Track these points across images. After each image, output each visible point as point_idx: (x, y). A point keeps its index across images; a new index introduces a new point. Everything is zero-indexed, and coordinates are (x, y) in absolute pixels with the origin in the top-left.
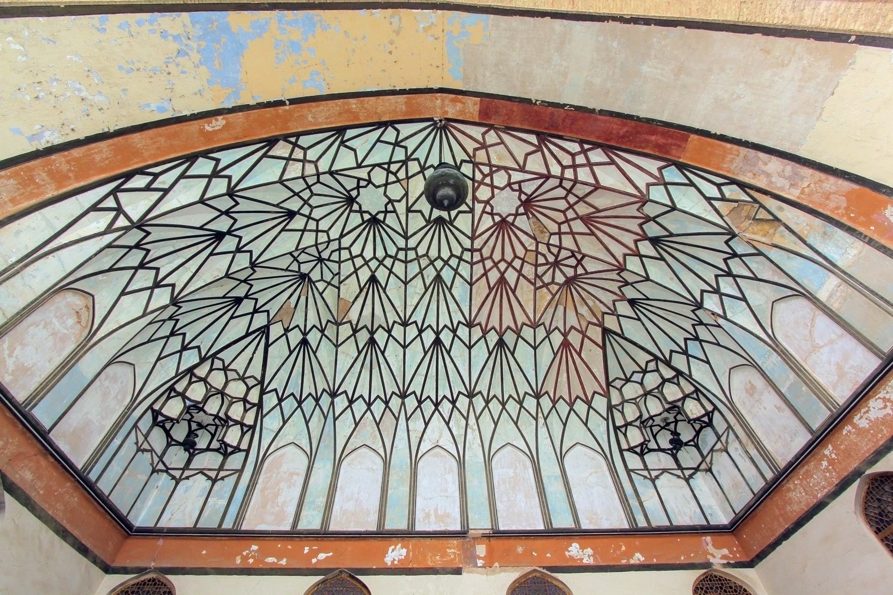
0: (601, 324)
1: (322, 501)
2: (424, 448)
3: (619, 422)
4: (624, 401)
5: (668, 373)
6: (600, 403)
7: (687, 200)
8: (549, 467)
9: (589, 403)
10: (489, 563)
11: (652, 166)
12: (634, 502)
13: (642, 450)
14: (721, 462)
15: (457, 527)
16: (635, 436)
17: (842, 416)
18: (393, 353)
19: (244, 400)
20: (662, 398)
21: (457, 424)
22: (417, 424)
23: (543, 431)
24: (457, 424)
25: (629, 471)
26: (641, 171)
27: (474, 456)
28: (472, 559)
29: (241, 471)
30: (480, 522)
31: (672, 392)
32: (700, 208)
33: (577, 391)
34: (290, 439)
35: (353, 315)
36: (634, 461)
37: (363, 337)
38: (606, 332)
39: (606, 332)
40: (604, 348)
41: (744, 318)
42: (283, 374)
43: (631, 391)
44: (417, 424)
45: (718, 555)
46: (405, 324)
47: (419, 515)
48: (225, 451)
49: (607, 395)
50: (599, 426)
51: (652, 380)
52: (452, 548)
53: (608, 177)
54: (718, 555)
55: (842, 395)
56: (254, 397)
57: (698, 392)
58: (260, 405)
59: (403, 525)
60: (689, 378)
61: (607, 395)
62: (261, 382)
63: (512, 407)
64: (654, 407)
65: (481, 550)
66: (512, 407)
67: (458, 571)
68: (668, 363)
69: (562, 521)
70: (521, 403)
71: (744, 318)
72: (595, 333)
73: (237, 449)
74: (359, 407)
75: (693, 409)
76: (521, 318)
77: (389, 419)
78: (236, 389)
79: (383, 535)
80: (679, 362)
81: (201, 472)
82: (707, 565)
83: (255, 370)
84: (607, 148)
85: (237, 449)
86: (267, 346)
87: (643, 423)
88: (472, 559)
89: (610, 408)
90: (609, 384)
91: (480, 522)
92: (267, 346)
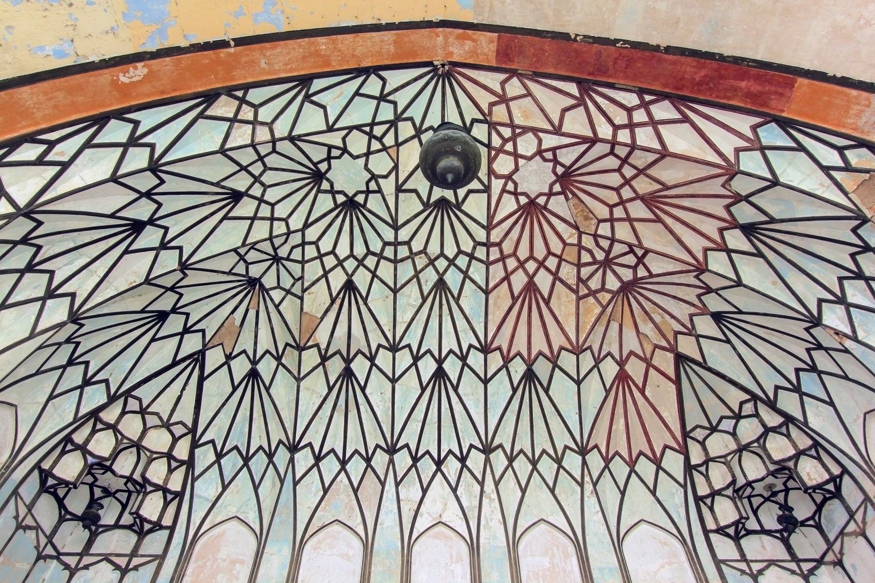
0: (672, 349)
5: (772, 420)
7: (795, 171)
11: (743, 123)
20: (764, 455)
21: (468, 490)
26: (726, 132)
31: (779, 447)
36: (725, 548)
38: (681, 359)
39: (681, 359)
43: (719, 444)
44: (411, 492)
51: (749, 430)
53: (680, 139)
57: (818, 447)
60: (804, 426)
61: (685, 451)
68: (772, 405)
72: (665, 361)
75: (811, 471)
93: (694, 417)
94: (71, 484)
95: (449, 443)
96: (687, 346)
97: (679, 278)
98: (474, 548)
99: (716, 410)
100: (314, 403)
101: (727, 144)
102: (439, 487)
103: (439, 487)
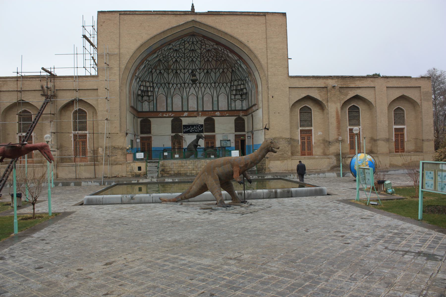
1: (171, 106)
2: (190, 94)
3: (232, 89)
4: (234, 85)
6: (229, 84)
8: (215, 99)
9: (227, 84)
10: (202, 115)
12: (230, 105)
13: (235, 95)
15: (196, 110)
16: (234, 92)
18: (182, 75)
19: (150, 86)
22: (188, 89)
23: (215, 91)
25: (231, 99)
27: (200, 96)
28: (198, 115)
29: (153, 100)
30: (200, 109)
33: (225, 81)
34: (161, 92)
35: (172, 67)
36: (233, 97)
37: (174, 71)
38: (233, 70)
39: (233, 70)
40: (232, 73)
42: (157, 79)
43: (236, 83)
44: (188, 89)
46: (184, 69)
47: (189, 107)
48: (149, 96)
49: (231, 83)
50: (228, 89)
51: (240, 82)
52: (195, 114)
54: (241, 114)
56: (151, 85)
58: (153, 86)
59: (186, 110)
61: (231, 83)
62: (152, 82)
65: (200, 113)
66: (209, 85)
67: (196, 117)
68: (153, 84)
70: (211, 84)
73: (151, 96)
74: (175, 85)
76: (212, 67)
77: (181, 88)
78: (148, 84)
79: (183, 112)
80: (155, 85)
81: (146, 100)
82: (239, 116)
83: (151, 80)
85: (151, 96)
86: (152, 74)
89: (231, 86)
90: (232, 81)
91: (200, 109)
92: (152, 74)
93: (233, 78)
95: (206, 81)
102: (192, 89)
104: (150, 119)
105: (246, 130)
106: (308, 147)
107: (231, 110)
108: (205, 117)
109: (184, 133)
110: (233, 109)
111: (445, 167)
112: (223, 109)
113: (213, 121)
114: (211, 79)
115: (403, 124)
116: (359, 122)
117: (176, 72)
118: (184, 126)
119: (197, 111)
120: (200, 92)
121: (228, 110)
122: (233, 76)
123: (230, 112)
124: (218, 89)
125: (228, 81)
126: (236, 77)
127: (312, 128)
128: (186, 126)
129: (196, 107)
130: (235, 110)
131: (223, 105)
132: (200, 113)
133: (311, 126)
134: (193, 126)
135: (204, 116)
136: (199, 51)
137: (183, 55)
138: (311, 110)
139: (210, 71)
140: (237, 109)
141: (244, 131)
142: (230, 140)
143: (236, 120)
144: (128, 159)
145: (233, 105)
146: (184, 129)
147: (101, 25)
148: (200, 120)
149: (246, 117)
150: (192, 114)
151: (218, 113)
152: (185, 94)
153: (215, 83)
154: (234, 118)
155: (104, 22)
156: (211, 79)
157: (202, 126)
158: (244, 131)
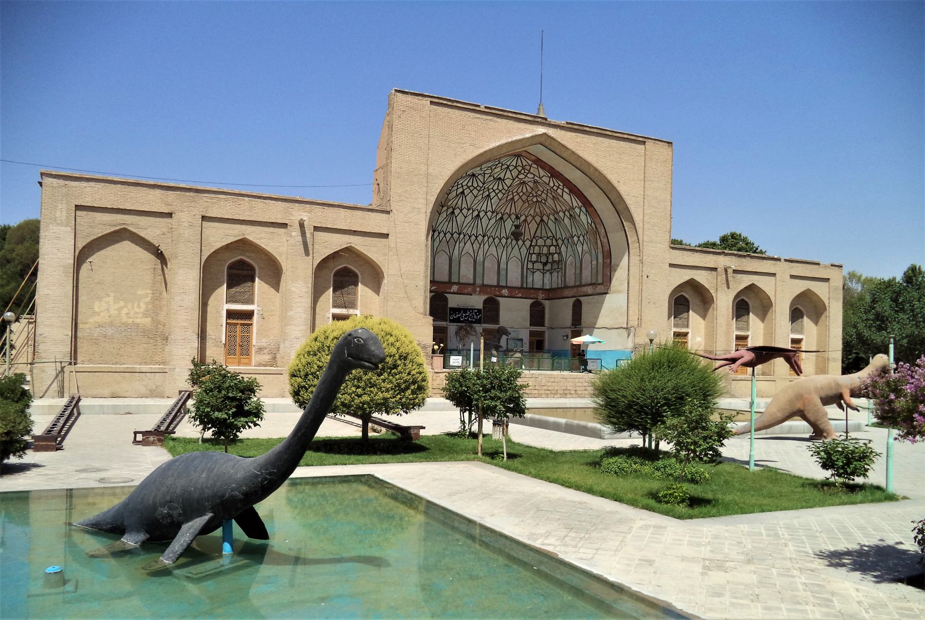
0: (542, 217)
5: (555, 243)
6: (528, 243)
7: (583, 217)
11: (580, 204)
13: (534, 263)
14: (555, 274)
16: (534, 258)
17: (581, 286)
18: (460, 218)
20: (549, 249)
21: (476, 246)
24: (476, 246)
26: (576, 203)
28: (475, 291)
30: (479, 282)
31: (553, 249)
32: (585, 222)
36: (530, 266)
37: (450, 210)
38: (542, 220)
39: (542, 220)
41: (580, 249)
43: (540, 242)
44: (462, 245)
45: (541, 296)
51: (549, 242)
53: (566, 197)
54: (541, 296)
55: (583, 283)
57: (560, 254)
59: (457, 281)
60: (560, 249)
61: (532, 241)
63: (497, 241)
64: (545, 250)
65: (478, 289)
68: (556, 240)
69: (503, 283)
71: (580, 249)
72: (538, 219)
75: (556, 257)
80: (560, 242)
84: (570, 191)
87: (539, 254)
88: (475, 291)
93: (538, 234)
94: (446, 345)
95: (474, 232)
96: (545, 218)
97: (518, 507)
98: (475, 261)
99: (544, 234)
100: (566, 553)
101: (575, 204)
102: (469, 243)
103: (469, 243)
104: (499, 298)
105: (547, 324)
106: (479, 359)
107: (526, 288)
108: (484, 297)
109: (451, 321)
110: (530, 286)
111: (1, 434)
112: (514, 285)
113: (497, 304)
114: (503, 230)
115: (801, 332)
116: (748, 325)
117: (453, 212)
118: (451, 309)
119: (474, 284)
120: (481, 252)
121: (522, 288)
122: (539, 231)
123: (523, 291)
124: (487, 246)
125: (503, 234)
126: (544, 231)
127: (689, 330)
128: (455, 310)
129: (471, 277)
130: (533, 289)
131: (514, 278)
132: (478, 289)
133: (687, 326)
134: (465, 310)
135: (484, 294)
136: (508, 182)
137: (481, 185)
138: (688, 301)
139: (505, 217)
140: (535, 286)
141: (543, 325)
142: (521, 340)
143: (532, 306)
144: (434, 365)
145: (530, 279)
146: (451, 314)
147: (400, 117)
148: (477, 301)
149: (547, 301)
150: (465, 288)
151: (505, 292)
152: (456, 252)
153: (507, 239)
154: (530, 301)
155: (404, 111)
156: (503, 230)
157: (479, 311)
158: (543, 325)
